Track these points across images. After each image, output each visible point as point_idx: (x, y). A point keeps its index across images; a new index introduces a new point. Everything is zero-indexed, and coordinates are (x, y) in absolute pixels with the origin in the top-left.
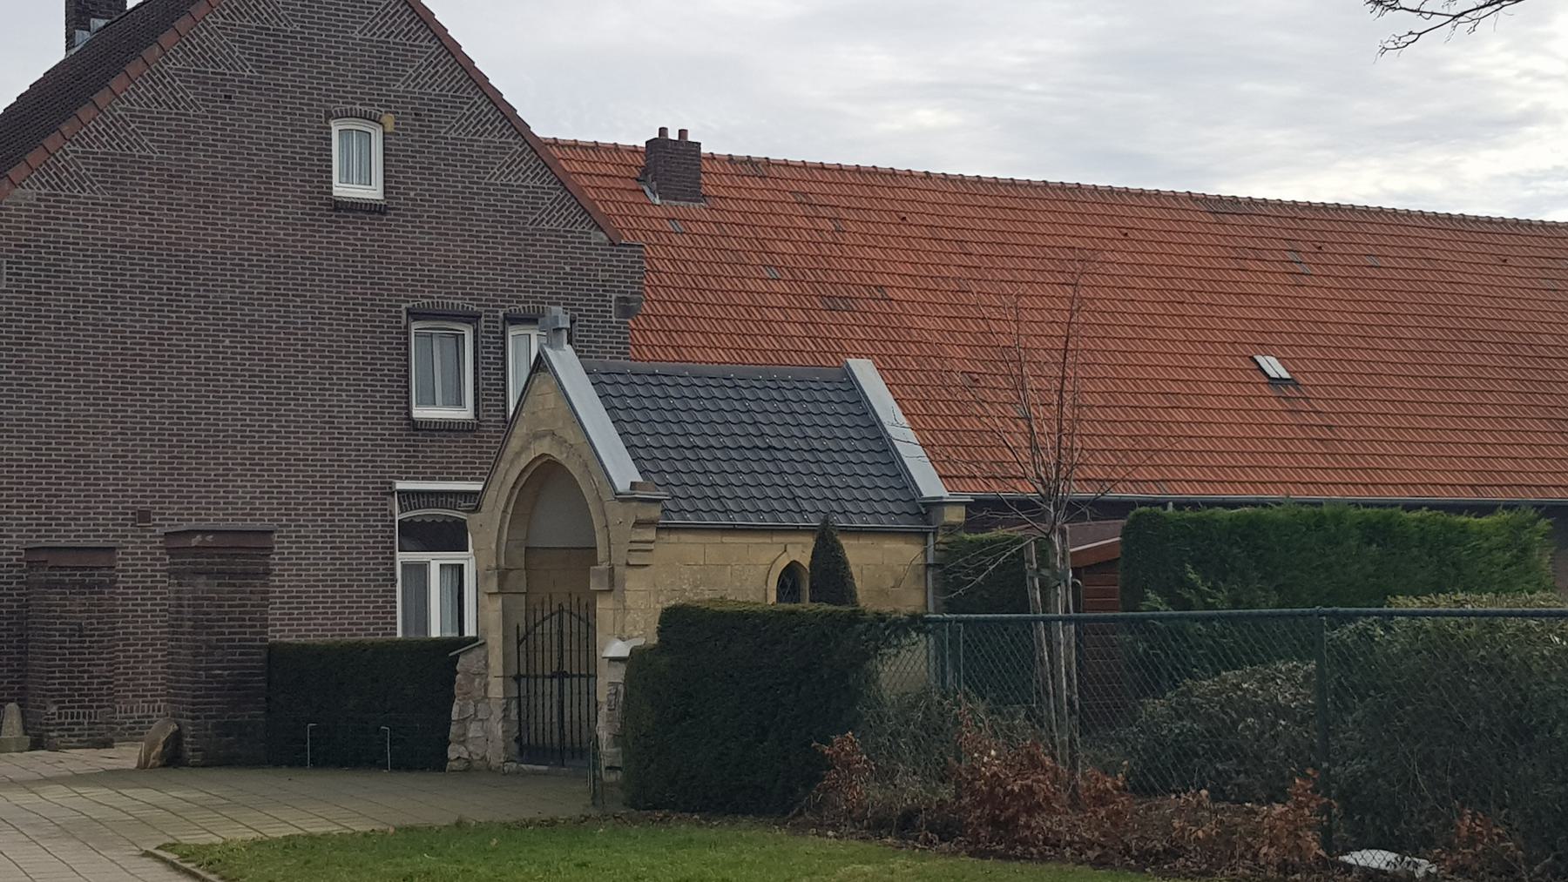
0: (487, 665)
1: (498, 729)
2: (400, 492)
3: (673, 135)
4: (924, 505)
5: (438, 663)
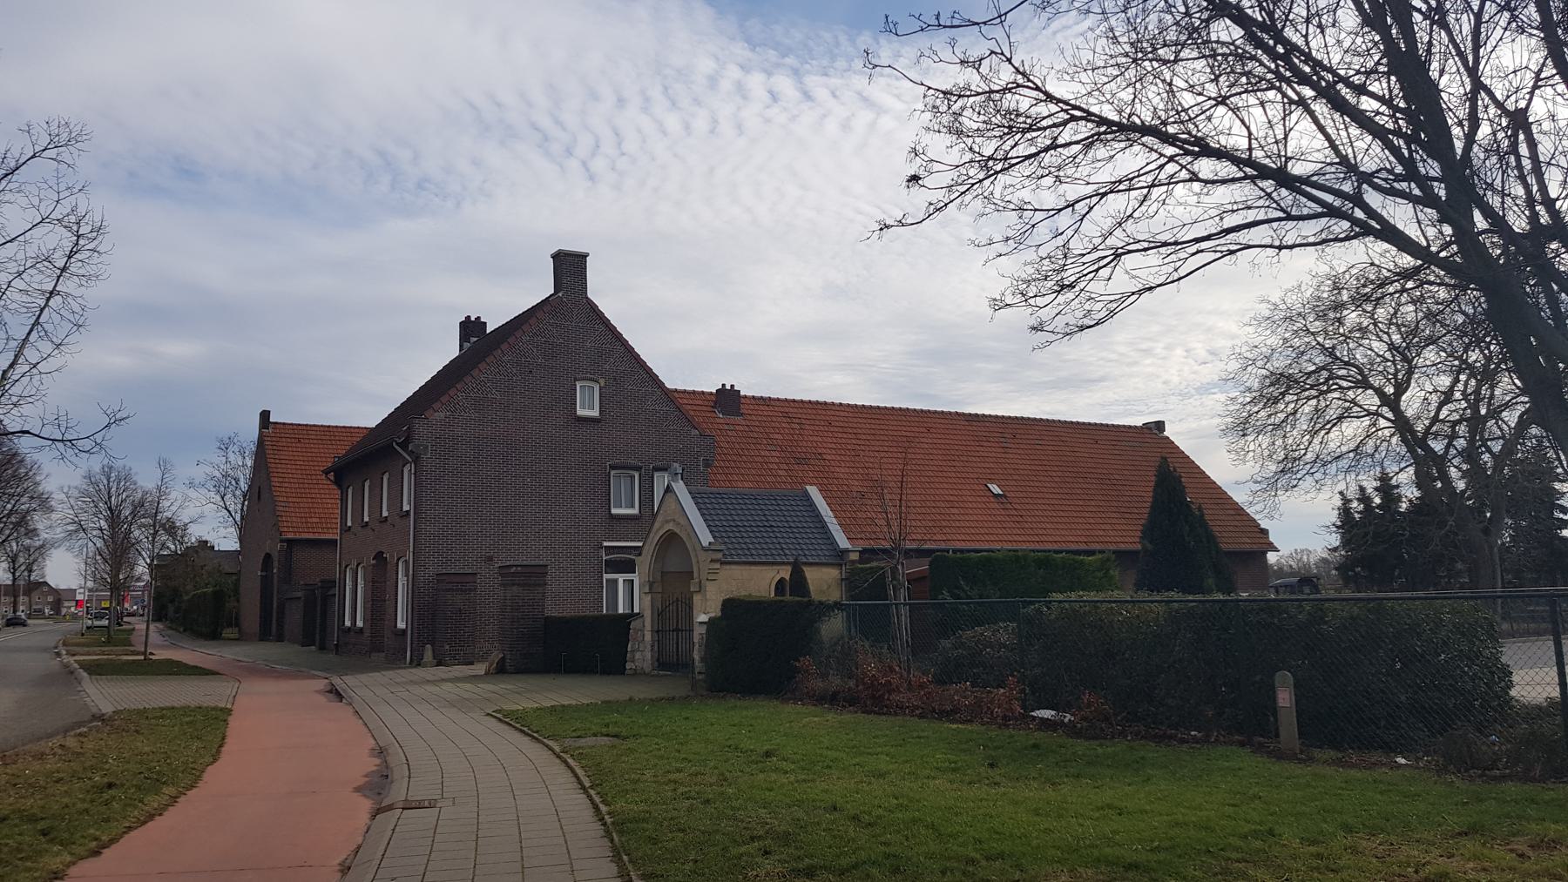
1: (648, 655)
5: (622, 625)
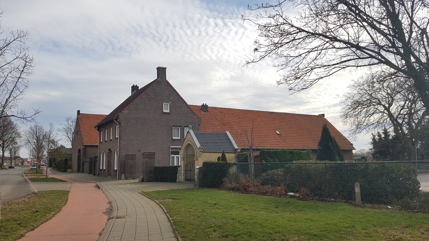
5: (175, 169)
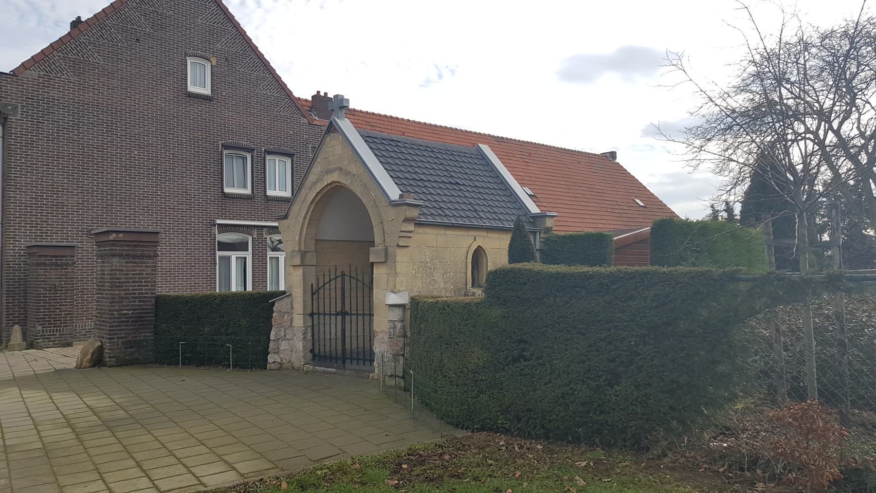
0: (292, 308)
1: (300, 345)
2: (218, 224)
3: (322, 94)
4: (532, 217)
5: (261, 306)
